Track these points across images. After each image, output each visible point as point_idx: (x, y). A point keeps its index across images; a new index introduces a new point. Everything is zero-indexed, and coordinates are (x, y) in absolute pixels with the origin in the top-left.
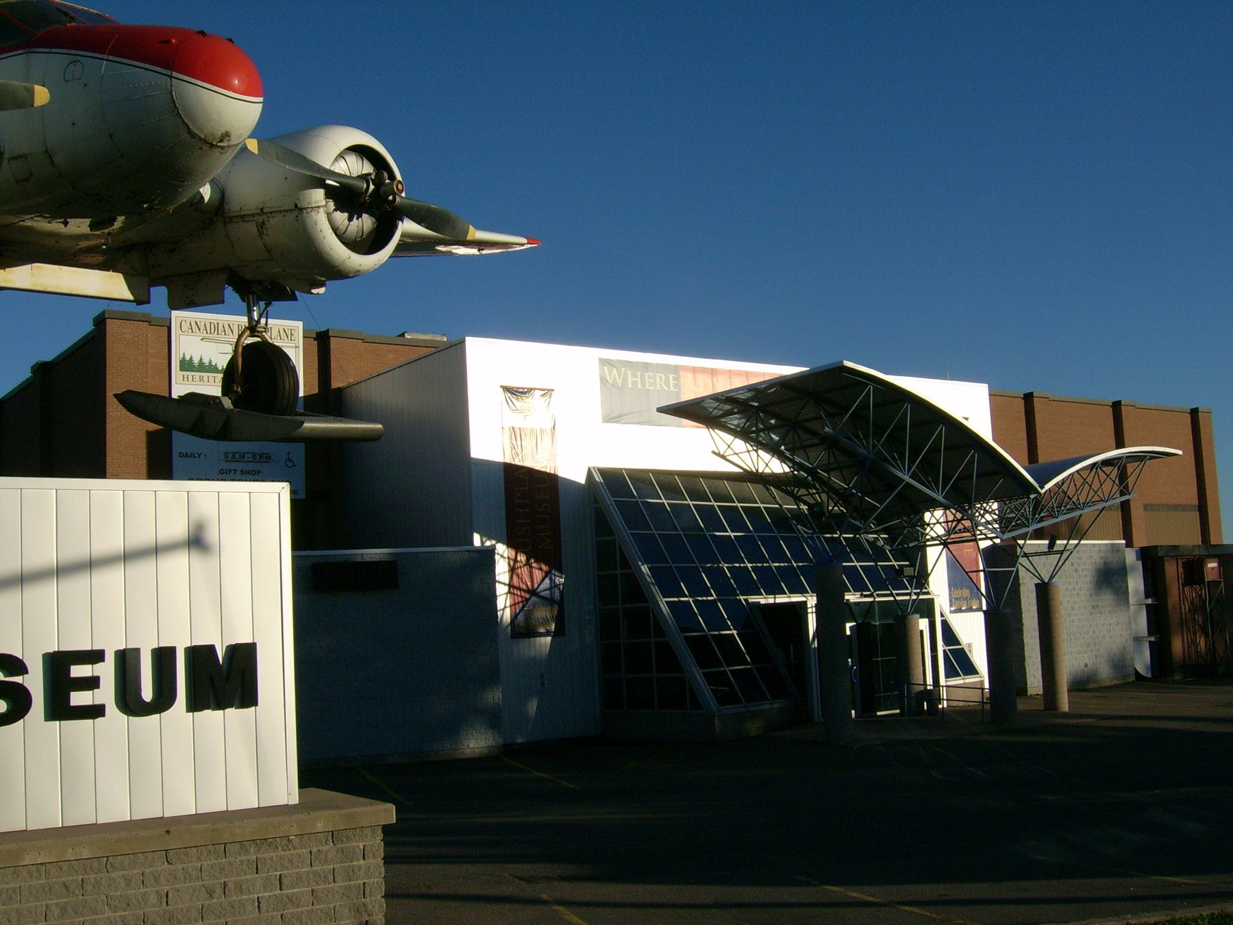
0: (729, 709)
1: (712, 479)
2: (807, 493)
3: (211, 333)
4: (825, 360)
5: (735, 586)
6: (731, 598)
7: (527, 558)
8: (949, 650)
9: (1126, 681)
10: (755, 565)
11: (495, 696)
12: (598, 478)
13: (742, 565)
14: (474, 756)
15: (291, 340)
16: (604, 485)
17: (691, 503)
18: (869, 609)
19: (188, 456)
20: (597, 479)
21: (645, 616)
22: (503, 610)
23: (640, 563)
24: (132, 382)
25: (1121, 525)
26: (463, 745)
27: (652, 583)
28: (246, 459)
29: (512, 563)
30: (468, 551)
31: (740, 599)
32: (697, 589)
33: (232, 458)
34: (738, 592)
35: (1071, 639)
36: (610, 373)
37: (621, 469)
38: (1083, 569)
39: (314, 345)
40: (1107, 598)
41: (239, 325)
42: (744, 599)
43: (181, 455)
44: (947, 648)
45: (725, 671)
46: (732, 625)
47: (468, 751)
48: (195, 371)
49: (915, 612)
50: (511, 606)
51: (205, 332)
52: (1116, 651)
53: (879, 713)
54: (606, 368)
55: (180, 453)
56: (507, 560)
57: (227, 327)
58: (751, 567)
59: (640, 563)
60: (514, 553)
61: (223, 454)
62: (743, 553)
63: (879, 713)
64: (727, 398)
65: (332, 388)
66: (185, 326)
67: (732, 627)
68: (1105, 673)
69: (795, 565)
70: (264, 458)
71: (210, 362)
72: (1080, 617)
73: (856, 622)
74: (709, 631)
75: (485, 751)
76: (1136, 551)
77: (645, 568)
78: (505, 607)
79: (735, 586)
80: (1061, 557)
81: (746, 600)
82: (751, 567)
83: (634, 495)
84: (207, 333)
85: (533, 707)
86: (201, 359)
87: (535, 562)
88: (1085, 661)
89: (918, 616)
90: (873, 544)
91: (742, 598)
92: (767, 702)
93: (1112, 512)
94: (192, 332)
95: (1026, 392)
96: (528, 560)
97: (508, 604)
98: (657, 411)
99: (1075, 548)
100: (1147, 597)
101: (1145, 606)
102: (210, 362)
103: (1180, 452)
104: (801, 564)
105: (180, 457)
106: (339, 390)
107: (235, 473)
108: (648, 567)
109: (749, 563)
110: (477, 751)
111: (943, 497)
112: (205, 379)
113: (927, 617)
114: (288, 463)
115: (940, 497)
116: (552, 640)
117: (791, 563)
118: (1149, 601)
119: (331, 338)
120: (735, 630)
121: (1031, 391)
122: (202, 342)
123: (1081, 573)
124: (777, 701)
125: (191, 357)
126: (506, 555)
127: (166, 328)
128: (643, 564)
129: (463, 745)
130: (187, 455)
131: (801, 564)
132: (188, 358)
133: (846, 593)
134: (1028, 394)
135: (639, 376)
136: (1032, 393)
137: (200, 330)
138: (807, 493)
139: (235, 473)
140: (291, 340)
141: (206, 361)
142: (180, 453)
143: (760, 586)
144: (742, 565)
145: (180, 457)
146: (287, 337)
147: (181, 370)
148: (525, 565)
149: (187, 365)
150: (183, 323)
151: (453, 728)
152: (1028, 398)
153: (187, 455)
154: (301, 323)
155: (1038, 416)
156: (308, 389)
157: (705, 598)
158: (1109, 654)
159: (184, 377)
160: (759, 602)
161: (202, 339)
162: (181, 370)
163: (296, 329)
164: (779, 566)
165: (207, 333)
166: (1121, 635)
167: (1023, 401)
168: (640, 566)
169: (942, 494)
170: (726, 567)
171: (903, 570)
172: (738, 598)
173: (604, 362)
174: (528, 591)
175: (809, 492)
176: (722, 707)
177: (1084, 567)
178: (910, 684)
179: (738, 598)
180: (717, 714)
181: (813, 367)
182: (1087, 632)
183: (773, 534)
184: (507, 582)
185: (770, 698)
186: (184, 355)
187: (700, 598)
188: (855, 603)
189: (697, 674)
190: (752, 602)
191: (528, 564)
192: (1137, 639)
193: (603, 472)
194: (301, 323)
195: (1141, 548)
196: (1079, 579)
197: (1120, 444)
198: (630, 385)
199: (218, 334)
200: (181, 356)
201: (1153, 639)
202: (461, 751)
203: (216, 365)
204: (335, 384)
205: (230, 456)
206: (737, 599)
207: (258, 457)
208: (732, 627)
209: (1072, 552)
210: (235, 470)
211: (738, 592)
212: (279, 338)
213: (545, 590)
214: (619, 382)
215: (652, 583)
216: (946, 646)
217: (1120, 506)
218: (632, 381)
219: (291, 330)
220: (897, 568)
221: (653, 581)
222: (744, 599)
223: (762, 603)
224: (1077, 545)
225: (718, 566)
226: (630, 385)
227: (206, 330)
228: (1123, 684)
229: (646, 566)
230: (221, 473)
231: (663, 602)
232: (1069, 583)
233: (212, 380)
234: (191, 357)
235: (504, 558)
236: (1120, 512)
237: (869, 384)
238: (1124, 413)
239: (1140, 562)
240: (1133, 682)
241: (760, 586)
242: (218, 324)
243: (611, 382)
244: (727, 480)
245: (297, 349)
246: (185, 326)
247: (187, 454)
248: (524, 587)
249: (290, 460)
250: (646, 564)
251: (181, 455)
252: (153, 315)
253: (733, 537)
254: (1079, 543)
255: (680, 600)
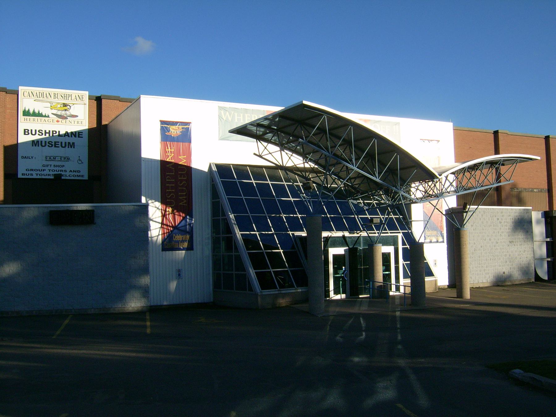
0: (266, 292)
1: (253, 167)
2: (317, 176)
3: (39, 97)
4: (292, 102)
5: (288, 226)
6: (284, 233)
7: (172, 210)
8: (405, 264)
9: (529, 282)
10: (303, 215)
11: (145, 280)
12: (214, 169)
13: (295, 215)
14: (134, 311)
15: (82, 100)
16: (217, 172)
17: (270, 183)
18: (356, 241)
19: (26, 158)
20: (214, 169)
21: (230, 241)
22: (158, 236)
23: (230, 213)
24: (3, 123)
25: (547, 200)
26: (128, 305)
27: (235, 224)
28: (57, 159)
29: (163, 212)
30: (138, 206)
31: (289, 234)
32: (262, 226)
33: (49, 159)
34: (289, 230)
35: (495, 258)
36: (225, 115)
37: (246, 166)
38: (505, 222)
39: (95, 103)
40: (520, 236)
41: (54, 93)
42: (292, 234)
43: (22, 157)
44: (404, 263)
45: (271, 271)
46: (280, 247)
47: (130, 308)
48: (30, 116)
49: (380, 243)
50: (162, 234)
51: (36, 97)
52: (524, 266)
53: (360, 296)
54: (222, 112)
55: (22, 157)
56: (161, 210)
57: (48, 94)
58: (300, 217)
59: (230, 213)
60: (165, 207)
61: (45, 157)
62: (296, 211)
63: (360, 296)
64: (257, 124)
65: (103, 124)
66: (26, 94)
67: (280, 248)
68: (517, 276)
69: (329, 216)
70: (66, 159)
71: (39, 112)
72: (502, 247)
73: (348, 247)
74: (265, 250)
75: (140, 309)
76: (541, 213)
77: (232, 216)
78: (159, 235)
79: (288, 226)
80: (467, 214)
81: (293, 234)
82: (300, 217)
83: (235, 178)
84: (37, 97)
85: (173, 285)
86: (34, 110)
87: (176, 212)
88: (503, 271)
89: (381, 244)
90: (356, 206)
91: (290, 233)
92: (293, 288)
93: (543, 193)
94: (77, 100)
95: (494, 131)
96: (173, 211)
97: (161, 233)
98: (229, 132)
99: (476, 210)
100: (547, 237)
101: (545, 242)
102: (39, 112)
103: (539, 158)
104: (332, 216)
105: (22, 158)
106: (106, 126)
107: (51, 167)
108: (234, 215)
109: (299, 214)
110: (136, 309)
111: (380, 180)
112: (36, 120)
113: (393, 246)
114: (79, 162)
115: (377, 179)
116: (185, 253)
117: (327, 215)
118: (548, 240)
119: (103, 100)
120: (282, 249)
121: (549, 135)
122: (35, 101)
123: (503, 224)
124: (300, 288)
125: (29, 109)
126: (160, 208)
127: (17, 95)
128: (231, 214)
129: (128, 305)
130: (25, 157)
131: (332, 216)
132: (27, 110)
133: (322, 232)
134: (495, 131)
135: (242, 116)
136: (549, 136)
137: (33, 96)
138: (317, 176)
139: (51, 167)
140: (82, 100)
141: (37, 111)
142: (22, 157)
143: (303, 226)
144: (295, 215)
145: (22, 158)
146: (80, 99)
147: (23, 116)
148: (171, 213)
149: (26, 113)
150: (25, 92)
151: (121, 296)
152: (547, 138)
153: (25, 157)
154: (88, 92)
155: (500, 143)
156: (91, 125)
157: (267, 233)
158: (518, 267)
159: (27, 119)
160: (301, 235)
161: (35, 100)
162: (23, 116)
163: (85, 95)
164: (286, 216)
165: (37, 97)
166: (527, 257)
167: (544, 140)
168: (229, 215)
169: (378, 178)
170: (284, 216)
171: (373, 220)
172: (288, 233)
173: (220, 108)
174: (172, 227)
175: (317, 175)
176: (263, 291)
177: (505, 221)
178: (374, 282)
179: (288, 233)
180: (259, 294)
181: (287, 106)
182: (506, 255)
183: (337, 201)
184: (160, 222)
185: (278, 288)
186: (25, 108)
187: (264, 233)
188: (348, 237)
189: (252, 272)
190: (296, 235)
191: (173, 213)
192: (542, 259)
193: (218, 166)
194: (88, 92)
195: (544, 211)
196: (501, 227)
197: (497, 152)
198: (236, 121)
199: (43, 98)
200: (24, 109)
201: (549, 259)
202: (127, 308)
203: (42, 113)
204: (104, 122)
205: (48, 158)
206: (287, 233)
207: (63, 158)
208: (280, 248)
209: (474, 212)
210: (51, 165)
211: (289, 230)
212: (75, 99)
213: (182, 227)
214: (230, 119)
215: (235, 224)
216: (404, 261)
217: (547, 190)
218: (237, 118)
219: (82, 96)
220: (370, 219)
221: (236, 223)
222: (292, 234)
223: (303, 235)
224: (477, 208)
225: (280, 216)
226: (236, 121)
227: (37, 96)
228: (528, 283)
229: (233, 215)
230: (43, 166)
231: (238, 234)
232: (495, 229)
233: (39, 120)
234: (29, 109)
235: (159, 209)
236: (547, 193)
237: (324, 115)
238: (551, 142)
239: (544, 219)
240: (533, 282)
241: (303, 226)
242: (43, 93)
243: (225, 119)
244: (280, 170)
245: (85, 105)
246: (26, 94)
247: (25, 157)
248: (171, 225)
249: (80, 160)
250: (233, 214)
251: (22, 157)
252: (8, 89)
253: (292, 201)
254: (478, 207)
255: (250, 233)
